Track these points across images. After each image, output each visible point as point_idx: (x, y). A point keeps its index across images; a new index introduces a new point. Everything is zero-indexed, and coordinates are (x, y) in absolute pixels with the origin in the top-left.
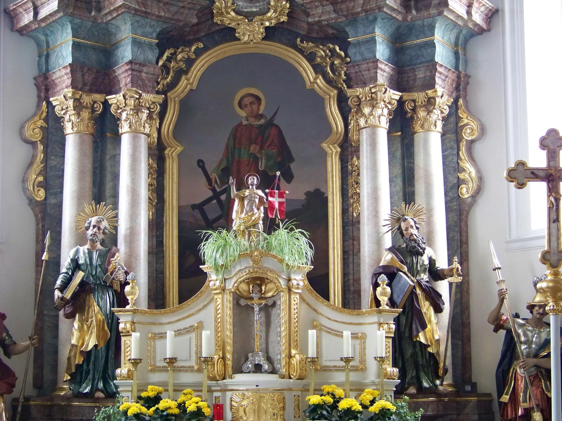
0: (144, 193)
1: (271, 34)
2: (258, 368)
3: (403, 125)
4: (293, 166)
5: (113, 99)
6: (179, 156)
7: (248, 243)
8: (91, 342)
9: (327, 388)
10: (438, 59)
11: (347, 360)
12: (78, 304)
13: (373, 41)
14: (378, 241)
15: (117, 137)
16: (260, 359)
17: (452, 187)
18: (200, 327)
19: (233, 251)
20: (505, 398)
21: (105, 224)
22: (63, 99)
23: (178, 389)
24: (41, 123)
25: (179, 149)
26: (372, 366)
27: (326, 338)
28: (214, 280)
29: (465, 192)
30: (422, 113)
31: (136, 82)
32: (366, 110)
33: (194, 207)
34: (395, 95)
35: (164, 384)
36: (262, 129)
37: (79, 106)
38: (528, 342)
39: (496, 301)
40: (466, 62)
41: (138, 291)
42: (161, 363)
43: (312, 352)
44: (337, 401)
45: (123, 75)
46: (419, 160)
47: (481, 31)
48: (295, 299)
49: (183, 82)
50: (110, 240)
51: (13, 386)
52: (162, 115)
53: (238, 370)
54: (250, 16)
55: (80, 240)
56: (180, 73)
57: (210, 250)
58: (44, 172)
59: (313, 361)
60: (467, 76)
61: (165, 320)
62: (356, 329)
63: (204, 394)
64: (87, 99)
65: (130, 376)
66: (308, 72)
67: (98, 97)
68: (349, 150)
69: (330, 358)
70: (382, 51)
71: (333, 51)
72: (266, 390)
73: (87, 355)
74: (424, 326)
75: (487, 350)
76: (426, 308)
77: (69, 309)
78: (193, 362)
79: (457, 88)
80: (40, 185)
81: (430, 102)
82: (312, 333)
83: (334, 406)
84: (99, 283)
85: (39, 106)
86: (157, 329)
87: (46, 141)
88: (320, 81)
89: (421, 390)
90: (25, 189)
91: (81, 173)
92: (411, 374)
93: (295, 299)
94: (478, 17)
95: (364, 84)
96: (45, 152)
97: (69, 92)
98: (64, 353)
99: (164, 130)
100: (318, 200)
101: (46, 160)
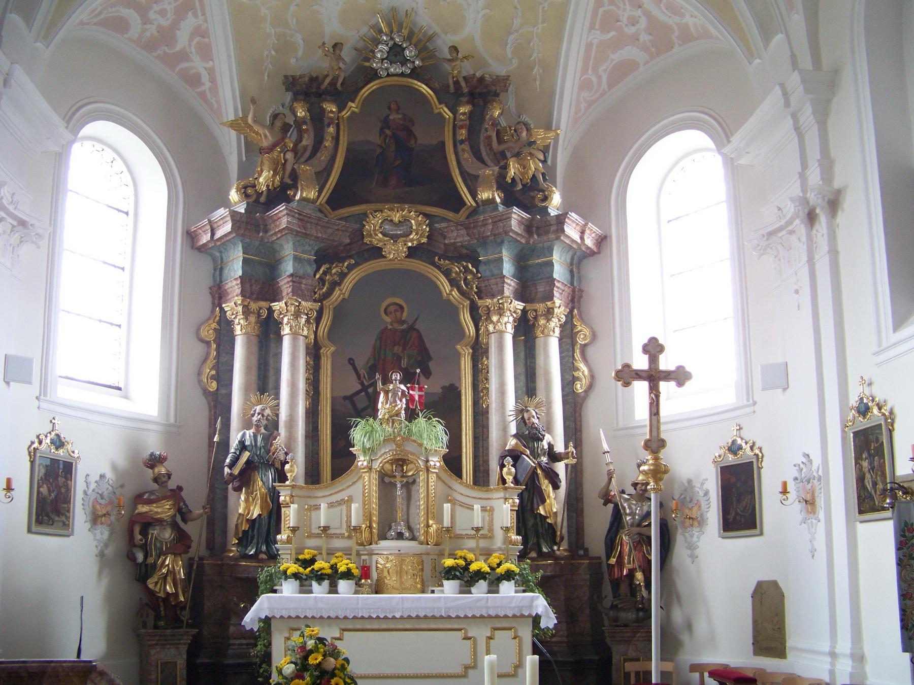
0: (302, 385)
1: (413, 252)
2: (400, 536)
4: (431, 365)
5: (276, 306)
8: (256, 512)
9: (460, 553)
10: (556, 276)
11: (478, 529)
12: (244, 479)
13: (500, 260)
14: (505, 428)
15: (280, 338)
16: (402, 528)
17: (568, 383)
18: (350, 500)
19: (379, 436)
20: (613, 561)
21: (268, 412)
22: (233, 306)
23: (331, 553)
24: (214, 325)
26: (499, 535)
27: (459, 510)
28: (362, 461)
29: (579, 388)
30: (542, 322)
31: (297, 292)
32: (495, 318)
33: (345, 398)
34: (520, 305)
36: (405, 333)
37: (247, 312)
38: (632, 514)
39: (606, 479)
40: (580, 279)
41: (296, 469)
43: (447, 522)
44: (468, 563)
45: (285, 286)
46: (540, 361)
48: (433, 478)
49: (337, 292)
50: (273, 425)
53: (383, 537)
54: (395, 238)
55: (247, 424)
56: (335, 285)
57: (358, 435)
58: (216, 367)
59: (448, 530)
60: (581, 291)
61: (320, 493)
62: (485, 503)
63: (353, 557)
64: (254, 306)
65: (289, 541)
66: (445, 286)
67: (263, 304)
68: (479, 351)
69: (462, 527)
70: (508, 268)
71: (466, 268)
73: (252, 522)
74: (543, 501)
75: (597, 521)
76: (546, 486)
77: (236, 484)
78: (344, 531)
79: (572, 301)
80: (213, 377)
81: (549, 312)
82: (447, 507)
83: (466, 569)
84: (262, 462)
85: (213, 311)
86: (313, 502)
87: (218, 341)
88: (455, 293)
89: (541, 555)
90: (200, 381)
91: (248, 369)
93: (433, 478)
94: (589, 242)
95: (493, 296)
97: (239, 300)
98: (232, 521)
99: (320, 332)
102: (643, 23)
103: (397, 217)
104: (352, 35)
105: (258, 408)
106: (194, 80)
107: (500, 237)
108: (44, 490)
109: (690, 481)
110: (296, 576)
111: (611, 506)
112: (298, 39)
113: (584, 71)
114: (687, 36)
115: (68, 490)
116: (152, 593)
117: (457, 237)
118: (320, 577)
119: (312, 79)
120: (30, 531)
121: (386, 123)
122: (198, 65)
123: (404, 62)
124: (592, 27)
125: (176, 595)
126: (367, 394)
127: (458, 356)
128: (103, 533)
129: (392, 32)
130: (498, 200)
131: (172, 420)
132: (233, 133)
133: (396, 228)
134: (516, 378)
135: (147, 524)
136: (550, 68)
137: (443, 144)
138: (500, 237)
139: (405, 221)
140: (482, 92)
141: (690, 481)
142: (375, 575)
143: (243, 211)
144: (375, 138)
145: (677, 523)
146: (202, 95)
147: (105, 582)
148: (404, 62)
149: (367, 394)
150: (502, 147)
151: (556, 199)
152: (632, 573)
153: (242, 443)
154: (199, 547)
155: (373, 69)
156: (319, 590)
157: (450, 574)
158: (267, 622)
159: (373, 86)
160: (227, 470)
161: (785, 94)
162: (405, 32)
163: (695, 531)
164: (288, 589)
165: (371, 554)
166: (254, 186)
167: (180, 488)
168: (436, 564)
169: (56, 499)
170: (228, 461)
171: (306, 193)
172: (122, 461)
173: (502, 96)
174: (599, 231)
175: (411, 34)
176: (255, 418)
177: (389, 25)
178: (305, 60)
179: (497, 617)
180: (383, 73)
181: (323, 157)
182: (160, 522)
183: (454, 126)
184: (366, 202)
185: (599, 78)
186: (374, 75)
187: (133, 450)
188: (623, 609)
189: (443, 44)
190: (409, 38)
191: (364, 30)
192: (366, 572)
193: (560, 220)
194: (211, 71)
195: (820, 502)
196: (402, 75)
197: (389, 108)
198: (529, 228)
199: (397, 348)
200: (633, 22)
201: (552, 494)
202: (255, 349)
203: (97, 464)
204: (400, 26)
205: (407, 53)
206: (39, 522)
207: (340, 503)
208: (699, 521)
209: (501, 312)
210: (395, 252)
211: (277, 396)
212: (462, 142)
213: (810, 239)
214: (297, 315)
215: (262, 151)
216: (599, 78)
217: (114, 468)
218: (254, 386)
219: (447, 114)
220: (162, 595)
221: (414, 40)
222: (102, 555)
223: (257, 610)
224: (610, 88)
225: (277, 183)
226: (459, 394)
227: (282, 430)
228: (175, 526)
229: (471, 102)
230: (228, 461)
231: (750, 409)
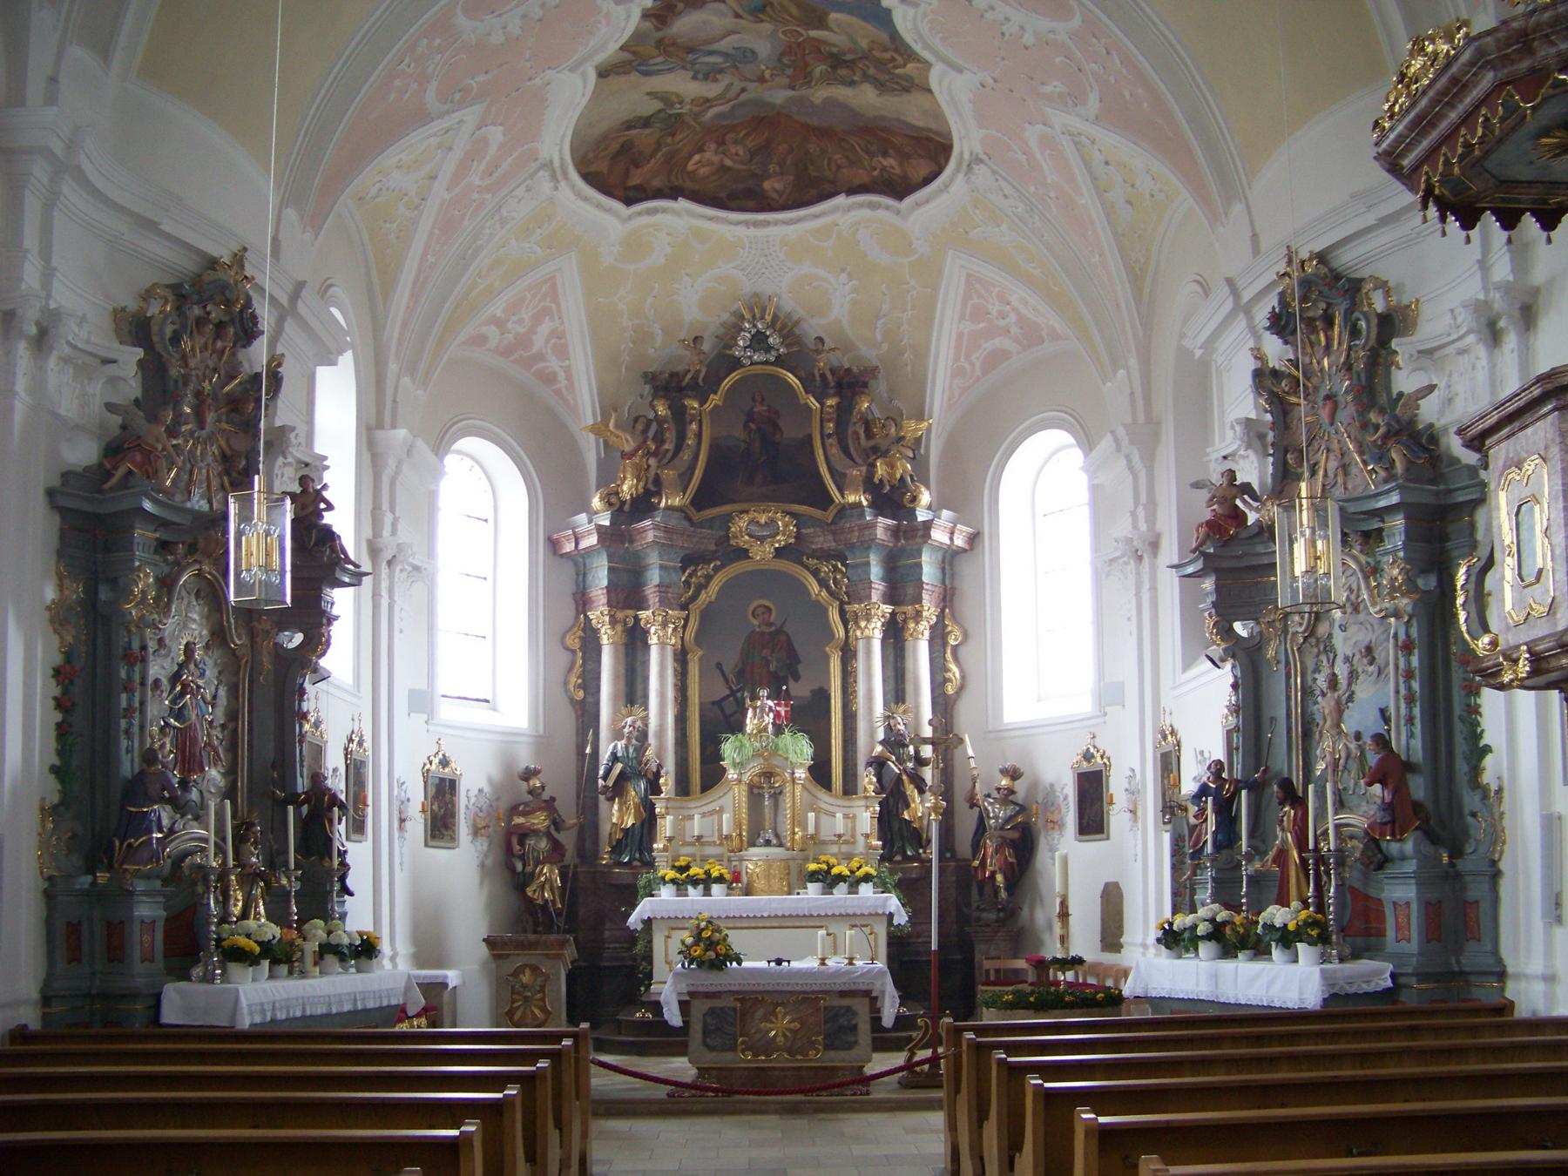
0: (670, 694)
1: (779, 553)
2: (768, 843)
3: (895, 634)
4: (800, 668)
5: (643, 614)
6: (700, 659)
7: (762, 734)
8: (630, 821)
9: (823, 858)
10: (925, 579)
11: (840, 836)
12: (618, 791)
13: (868, 564)
14: (872, 733)
15: (647, 647)
16: (769, 835)
17: (938, 684)
18: (721, 811)
19: (748, 751)
20: (977, 863)
21: (639, 723)
22: (599, 614)
23: (704, 859)
24: (580, 633)
25: (700, 653)
26: (861, 840)
27: (824, 819)
28: (732, 774)
29: (950, 690)
30: (912, 625)
31: (664, 603)
32: (863, 624)
33: (714, 703)
34: (888, 609)
35: (692, 855)
36: (773, 635)
37: (613, 622)
38: (996, 818)
39: (970, 784)
40: (952, 575)
41: (667, 783)
42: (689, 839)
43: (811, 830)
44: (830, 867)
45: (651, 592)
46: (909, 664)
47: (965, 551)
48: (798, 789)
49: (703, 596)
50: (643, 736)
51: (563, 855)
52: (685, 627)
53: (752, 844)
54: (762, 539)
55: (617, 735)
56: (701, 587)
57: (729, 749)
58: (582, 675)
59: (812, 837)
60: (953, 589)
61: (692, 805)
62: (847, 811)
63: (725, 862)
64: (620, 615)
65: (665, 849)
66: (814, 587)
67: (630, 612)
68: (848, 654)
69: (826, 834)
70: (876, 571)
71: (835, 567)
72: (774, 860)
73: (626, 831)
74: (907, 806)
75: (966, 824)
76: (911, 790)
77: (609, 794)
78: (715, 839)
79: (944, 600)
80: (580, 686)
81: (918, 616)
82: (811, 815)
83: (828, 872)
84: (635, 772)
85: (577, 617)
86: (686, 813)
87: (583, 648)
88: (824, 593)
89: (906, 858)
90: (567, 691)
91: (616, 678)
92: (898, 844)
93: (798, 789)
94: (959, 541)
95: (861, 601)
96: (583, 658)
97: (605, 610)
98: (605, 829)
99: (687, 637)
100: (823, 696)
101: (583, 665)
102: (1013, 317)
103: (763, 519)
104: (713, 321)
105: (629, 720)
106: (549, 379)
107: (867, 544)
108: (435, 807)
109: (1052, 786)
110: (673, 881)
111: (976, 809)
112: (657, 329)
113: (957, 359)
114: (1055, 336)
115: (454, 805)
116: (530, 901)
117: (822, 541)
118: (695, 882)
119: (673, 375)
120: (426, 845)
121: (750, 416)
122: (554, 364)
123: (769, 349)
124: (962, 318)
125: (554, 902)
126: (736, 699)
127: (827, 659)
128: (483, 845)
129: (754, 317)
130: (865, 503)
131: (541, 731)
132: (592, 437)
133: (763, 530)
134: (884, 681)
135: (524, 835)
136: (922, 353)
137: (810, 438)
138: (867, 544)
139: (773, 521)
140: (849, 384)
141: (1052, 786)
142: (745, 879)
143: (607, 523)
144: (738, 432)
145: (1040, 824)
146: (558, 393)
147: (486, 891)
148: (769, 349)
149: (736, 699)
150: (871, 443)
151: (925, 498)
152: (993, 874)
153: (614, 754)
154: (570, 856)
155: (734, 357)
156: (694, 893)
157: (813, 877)
158: (648, 923)
159: (735, 376)
160: (601, 782)
161: (1116, 440)
162: (768, 318)
163: (1056, 835)
164: (666, 893)
165: (741, 860)
166: (617, 493)
167: (553, 799)
168: (801, 868)
169: (444, 817)
170: (601, 773)
171: (672, 500)
172: (497, 775)
173: (872, 383)
174: (970, 530)
175: (775, 318)
176: (626, 730)
177: (751, 310)
178: (662, 351)
179: (855, 915)
180: (746, 362)
181: (686, 455)
182: (536, 832)
183: (822, 421)
184: (734, 502)
185: (972, 365)
186: (736, 364)
187: (507, 763)
188: (983, 910)
189: (812, 328)
190: (772, 325)
191: (725, 316)
192: (737, 877)
193: (927, 525)
194: (567, 370)
195: (1139, 813)
196: (766, 363)
197: (754, 399)
198: (895, 533)
199: (766, 659)
200: (1003, 316)
201: (918, 800)
202: (622, 657)
203: (475, 780)
204: (764, 310)
205: (771, 340)
206: (433, 837)
207: (711, 813)
208: (1058, 825)
209: (868, 618)
210: (762, 553)
211: (646, 709)
212: (830, 436)
213: (1138, 574)
214: (664, 625)
215: (624, 455)
216: (972, 365)
217: (490, 781)
218: (622, 701)
219: (813, 403)
220: (540, 902)
221: (778, 326)
222: (482, 865)
223: (641, 912)
224: (984, 374)
225: (641, 490)
226: (828, 698)
227: (652, 740)
228: (548, 835)
229: (838, 394)
230: (601, 773)
231: (1101, 720)
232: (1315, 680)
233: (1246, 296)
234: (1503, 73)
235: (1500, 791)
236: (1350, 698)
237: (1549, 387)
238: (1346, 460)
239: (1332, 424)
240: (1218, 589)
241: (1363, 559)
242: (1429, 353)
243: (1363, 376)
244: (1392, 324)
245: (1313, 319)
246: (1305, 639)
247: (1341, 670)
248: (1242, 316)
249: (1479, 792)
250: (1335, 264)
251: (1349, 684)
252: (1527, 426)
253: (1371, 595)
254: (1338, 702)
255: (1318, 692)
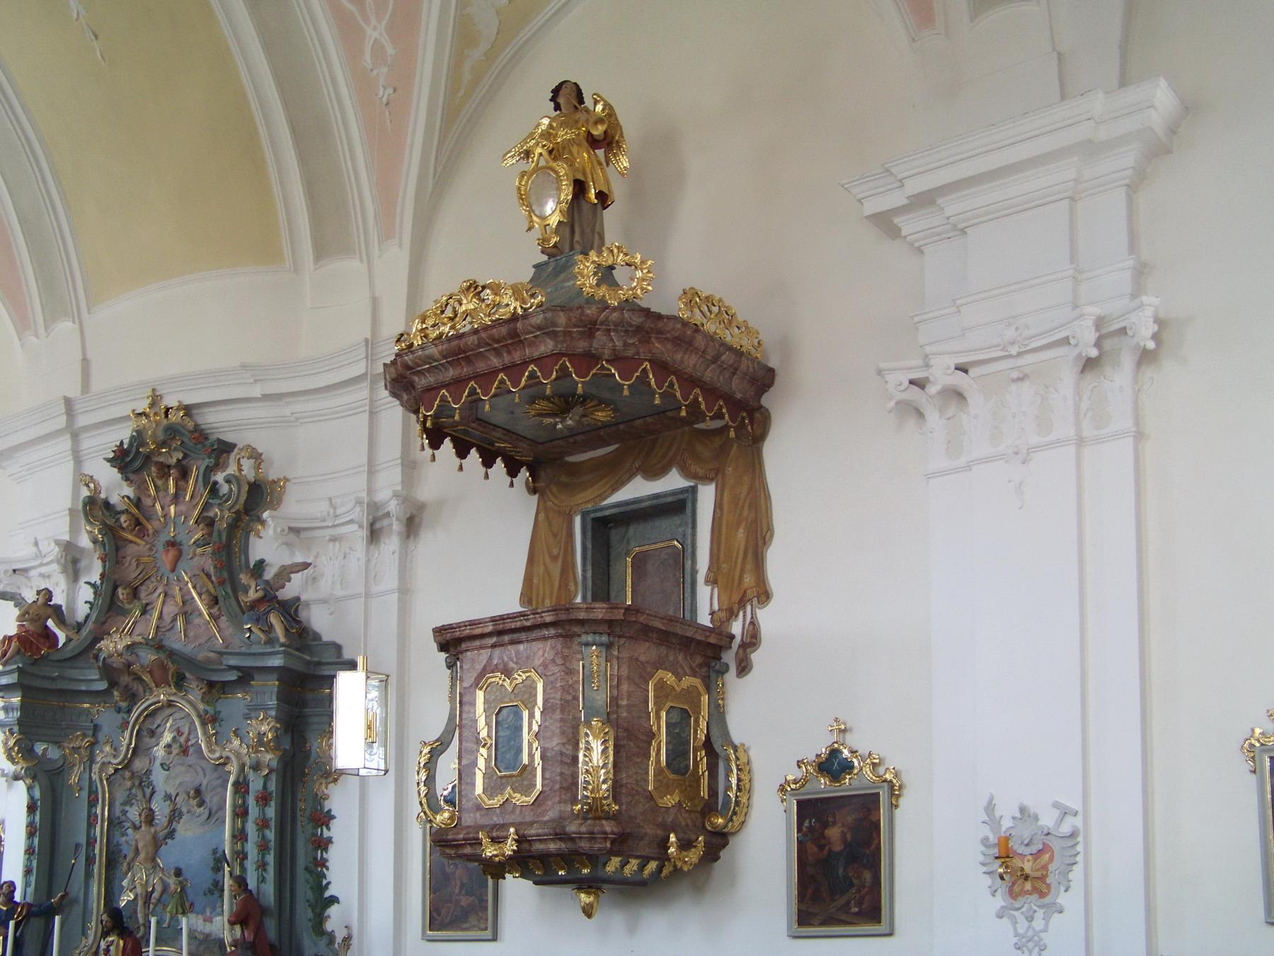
232: (125, 813)
233: (82, 421)
234: (562, 347)
235: (347, 940)
236: (171, 834)
237: (563, 616)
238: (188, 608)
239: (173, 570)
240: (23, 706)
241: (201, 707)
242: (295, 531)
243: (224, 537)
244: (259, 495)
245: (169, 467)
246: (116, 770)
247: (160, 808)
248: (68, 436)
249: (324, 940)
250: (200, 420)
251: (170, 822)
252: (520, 642)
253: (209, 743)
254: (155, 838)
255: (127, 825)
